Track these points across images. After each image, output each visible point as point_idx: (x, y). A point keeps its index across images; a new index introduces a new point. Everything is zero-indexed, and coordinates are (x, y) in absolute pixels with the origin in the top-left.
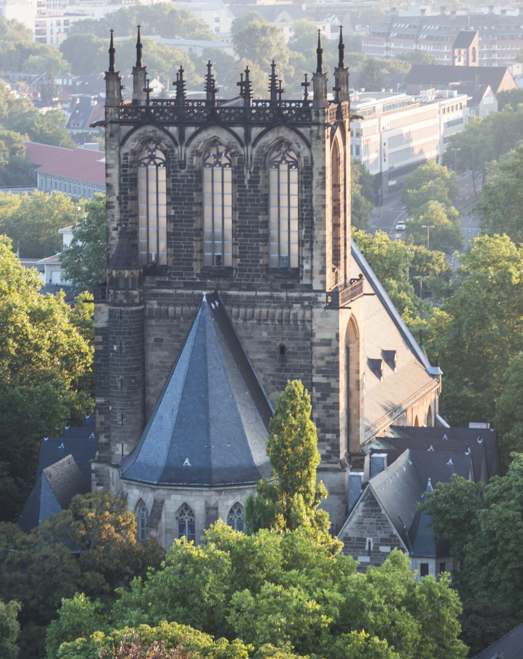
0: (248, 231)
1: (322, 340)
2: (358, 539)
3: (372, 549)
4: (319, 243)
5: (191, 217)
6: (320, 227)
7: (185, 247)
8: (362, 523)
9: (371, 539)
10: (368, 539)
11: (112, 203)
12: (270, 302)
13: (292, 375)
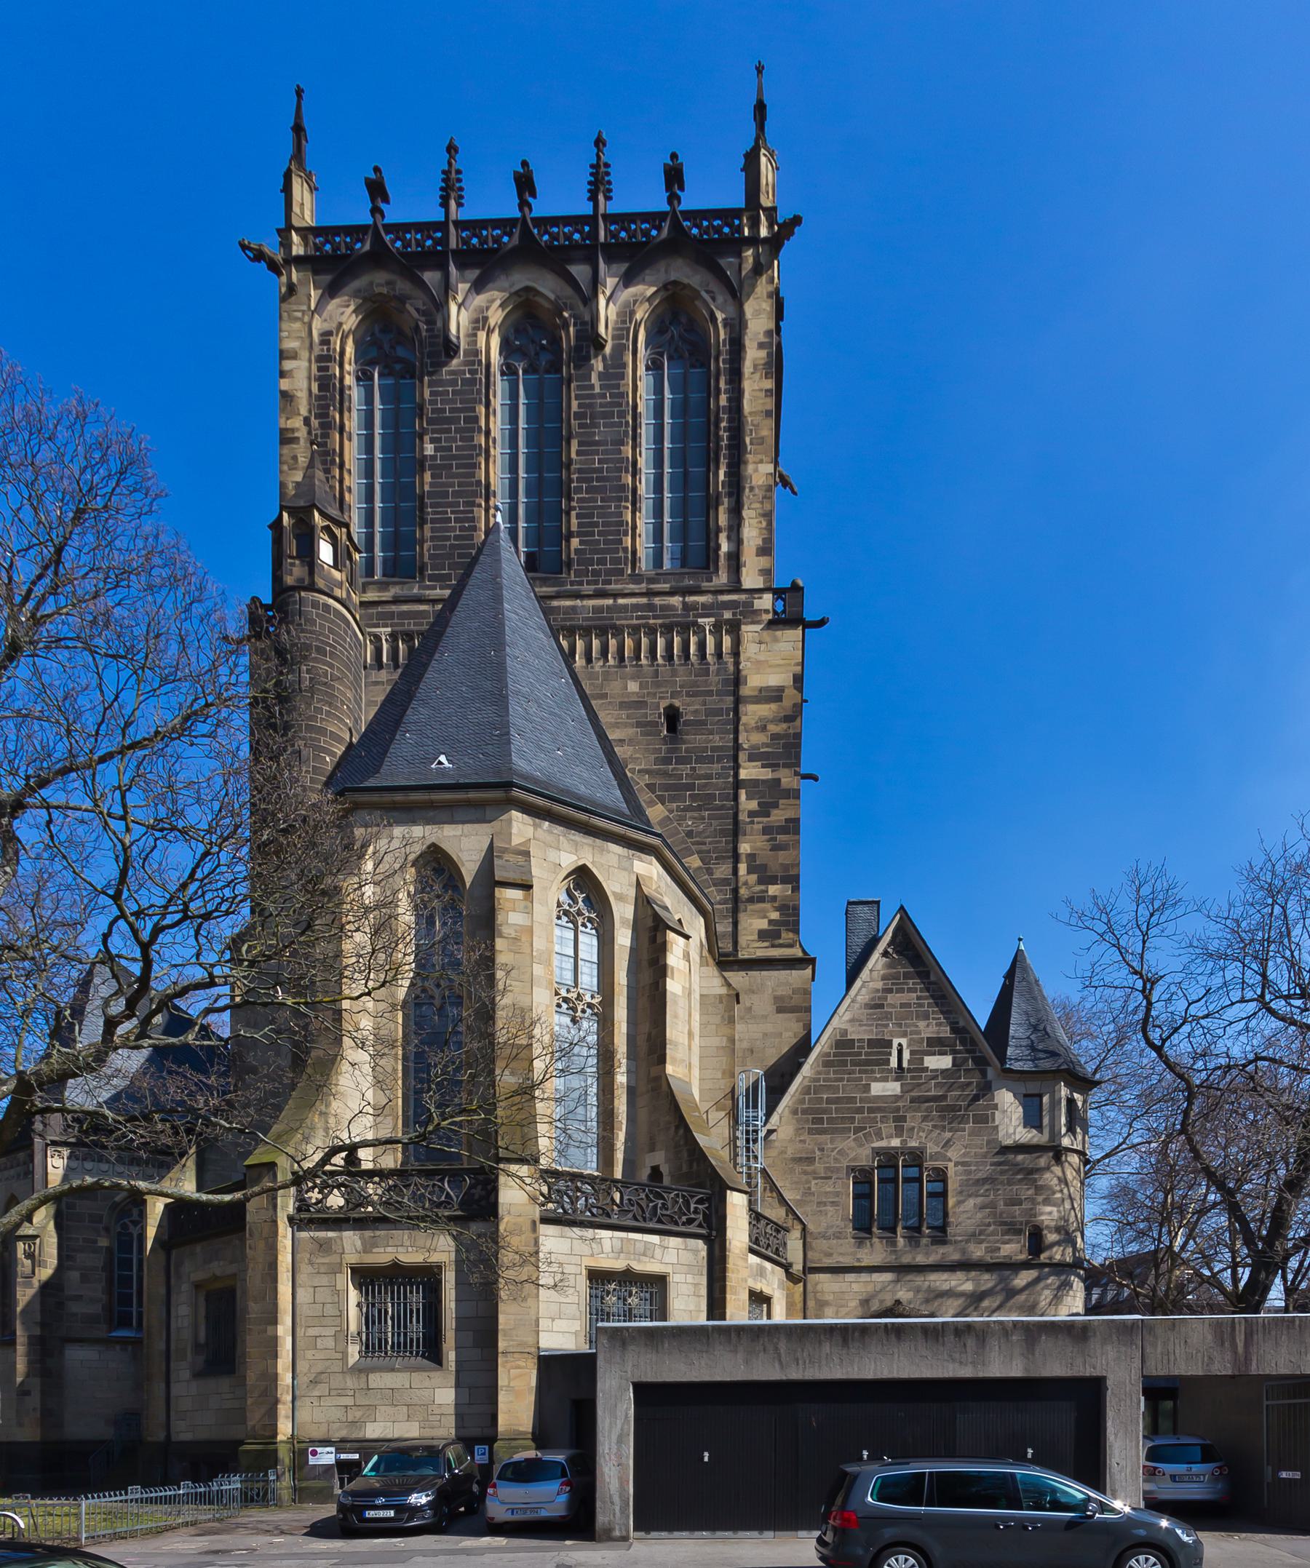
0: (598, 479)
1: (761, 690)
2: (871, 1043)
3: (905, 1065)
4: (757, 491)
5: (471, 457)
6: (760, 457)
7: (457, 520)
8: (881, 1006)
9: (904, 1041)
10: (896, 1042)
11: (293, 430)
12: (648, 618)
13: (693, 769)
